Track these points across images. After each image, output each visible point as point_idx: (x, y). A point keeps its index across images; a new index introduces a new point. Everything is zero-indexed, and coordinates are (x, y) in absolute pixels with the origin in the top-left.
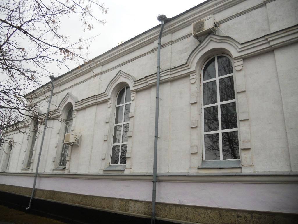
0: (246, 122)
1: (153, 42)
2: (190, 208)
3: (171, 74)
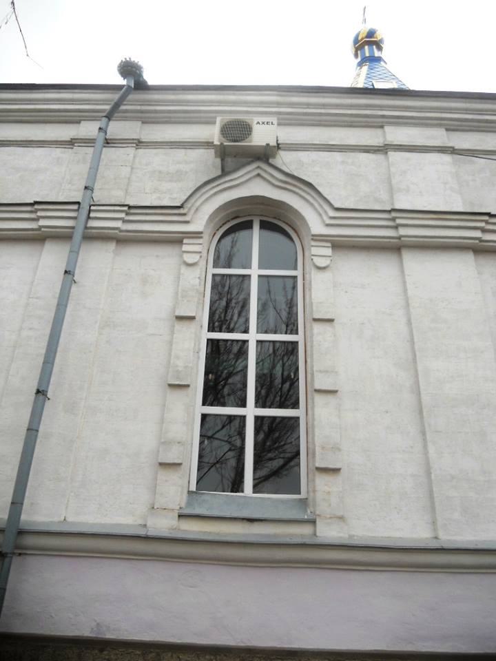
0: (330, 398)
1: (79, 122)
2: (138, 652)
3: (124, 221)
